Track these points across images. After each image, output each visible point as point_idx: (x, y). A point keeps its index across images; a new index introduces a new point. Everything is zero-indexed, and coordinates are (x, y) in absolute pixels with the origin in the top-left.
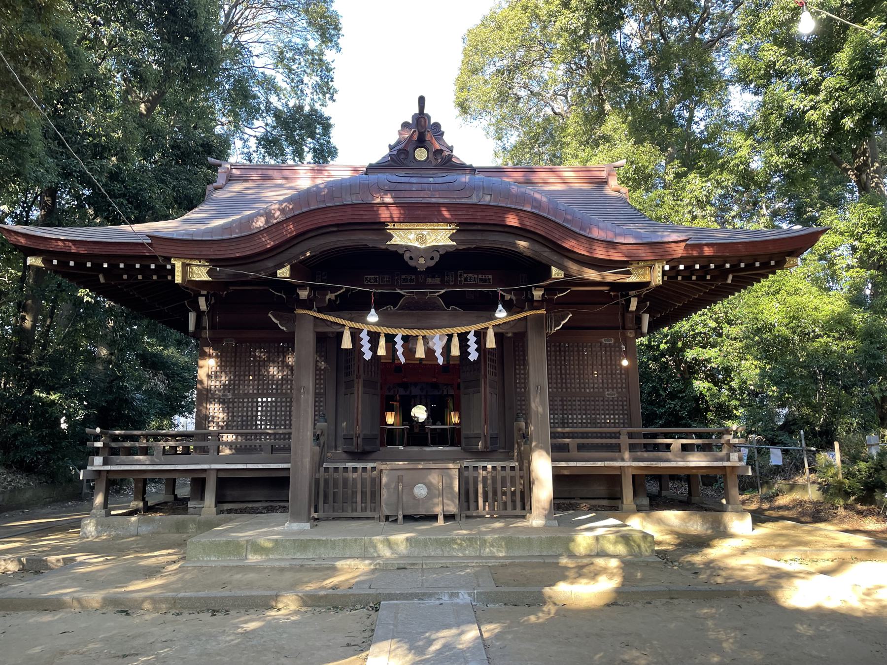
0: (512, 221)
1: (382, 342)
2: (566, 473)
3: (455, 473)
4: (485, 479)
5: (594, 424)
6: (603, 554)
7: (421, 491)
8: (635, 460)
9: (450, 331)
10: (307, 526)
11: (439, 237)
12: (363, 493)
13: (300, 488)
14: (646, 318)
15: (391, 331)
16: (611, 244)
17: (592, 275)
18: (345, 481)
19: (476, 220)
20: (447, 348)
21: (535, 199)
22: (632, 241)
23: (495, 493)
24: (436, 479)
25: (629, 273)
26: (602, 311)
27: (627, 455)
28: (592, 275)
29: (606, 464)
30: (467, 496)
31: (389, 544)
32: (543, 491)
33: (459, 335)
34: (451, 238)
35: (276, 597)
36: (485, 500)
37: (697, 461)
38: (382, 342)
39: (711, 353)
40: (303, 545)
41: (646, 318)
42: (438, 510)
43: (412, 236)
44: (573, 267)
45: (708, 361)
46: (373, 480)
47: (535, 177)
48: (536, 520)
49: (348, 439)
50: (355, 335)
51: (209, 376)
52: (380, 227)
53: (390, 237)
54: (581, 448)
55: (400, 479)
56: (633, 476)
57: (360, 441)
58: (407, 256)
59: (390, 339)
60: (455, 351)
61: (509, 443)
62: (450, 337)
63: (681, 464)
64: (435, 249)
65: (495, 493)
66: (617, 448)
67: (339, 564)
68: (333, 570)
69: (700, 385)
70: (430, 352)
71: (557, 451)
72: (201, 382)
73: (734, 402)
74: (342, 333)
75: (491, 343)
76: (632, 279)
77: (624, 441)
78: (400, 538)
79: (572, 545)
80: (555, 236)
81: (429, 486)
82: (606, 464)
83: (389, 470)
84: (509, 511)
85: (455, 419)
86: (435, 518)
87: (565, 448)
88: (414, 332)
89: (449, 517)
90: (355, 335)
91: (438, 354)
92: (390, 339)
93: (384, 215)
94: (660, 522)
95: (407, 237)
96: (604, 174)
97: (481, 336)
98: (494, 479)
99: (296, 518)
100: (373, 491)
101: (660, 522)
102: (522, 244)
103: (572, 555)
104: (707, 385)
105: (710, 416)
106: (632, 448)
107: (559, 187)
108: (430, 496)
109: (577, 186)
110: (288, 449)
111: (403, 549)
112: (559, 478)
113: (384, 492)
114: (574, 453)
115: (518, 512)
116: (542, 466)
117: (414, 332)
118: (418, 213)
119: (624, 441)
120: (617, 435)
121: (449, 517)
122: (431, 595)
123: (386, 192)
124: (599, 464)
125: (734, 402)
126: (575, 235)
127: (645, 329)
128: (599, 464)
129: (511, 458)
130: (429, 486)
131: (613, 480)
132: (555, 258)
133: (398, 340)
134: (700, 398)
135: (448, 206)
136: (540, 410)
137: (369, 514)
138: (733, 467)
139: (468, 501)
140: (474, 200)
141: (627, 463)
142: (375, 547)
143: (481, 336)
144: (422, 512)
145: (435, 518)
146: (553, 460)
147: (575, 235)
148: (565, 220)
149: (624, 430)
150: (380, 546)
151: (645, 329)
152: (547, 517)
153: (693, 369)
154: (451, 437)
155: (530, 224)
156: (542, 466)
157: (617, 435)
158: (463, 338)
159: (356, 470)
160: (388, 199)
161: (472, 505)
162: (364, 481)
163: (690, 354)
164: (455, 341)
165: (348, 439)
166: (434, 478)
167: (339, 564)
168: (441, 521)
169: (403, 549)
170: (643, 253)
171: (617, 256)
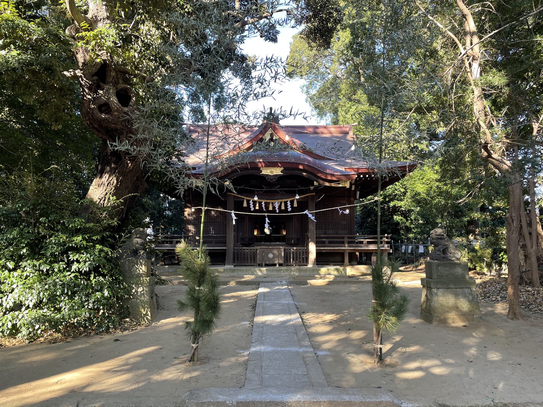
0: (301, 167)
1: (257, 205)
2: (324, 251)
3: (283, 250)
4: (293, 252)
5: (337, 234)
6: (329, 274)
7: (271, 256)
8: (350, 247)
9: (281, 201)
10: (233, 266)
11: (277, 171)
12: (251, 258)
13: (230, 256)
14: (358, 193)
15: (260, 201)
16: (332, 175)
17: (327, 184)
18: (244, 253)
19: (290, 168)
20: (280, 206)
21: (308, 160)
22: (339, 174)
23: (297, 258)
24: (276, 252)
25: (339, 184)
26: (335, 195)
27: (346, 245)
28: (327, 184)
29: (339, 248)
30: (287, 259)
31: (261, 271)
32: (312, 256)
33: (284, 202)
34: (281, 172)
35: (229, 282)
36: (293, 260)
37: (372, 247)
38: (257, 205)
39: (401, 204)
40: (233, 271)
41: (358, 193)
42: (276, 262)
43: (269, 171)
44: (321, 182)
45: (401, 207)
46: (254, 253)
47: (319, 131)
48: (310, 265)
49: (243, 239)
50: (248, 202)
51: (189, 215)
52: (259, 170)
53: (261, 172)
54: (330, 242)
55: (263, 252)
56: (349, 253)
57: (247, 240)
58: (267, 178)
59: (260, 204)
60: (283, 208)
61: (303, 242)
62: (281, 203)
63: (366, 248)
64: (276, 175)
65: (297, 258)
66: (343, 243)
67: (245, 276)
68: (243, 277)
69: (397, 218)
70: (274, 208)
71: (318, 244)
72: (186, 217)
73: (412, 226)
74: (243, 201)
75: (295, 205)
76: (340, 186)
77: (346, 240)
78: (264, 269)
79: (320, 272)
80: (315, 172)
81: (274, 254)
82: (339, 248)
83: (259, 249)
84: (302, 264)
85: (285, 233)
86: (275, 265)
87: (324, 242)
88: (268, 201)
89: (280, 265)
90: (248, 202)
91: (277, 209)
92: (260, 204)
93: (260, 165)
94: (357, 269)
95: (266, 171)
96: (347, 129)
97: (292, 202)
98: (296, 253)
99: (229, 264)
100: (255, 255)
101: (357, 269)
102: (304, 174)
103: (319, 274)
104: (400, 217)
105: (402, 232)
106: (349, 243)
107: (328, 135)
108: (274, 257)
109: (335, 135)
110: (226, 243)
111: (265, 272)
112: (318, 253)
113: (258, 256)
114: (327, 244)
115: (305, 264)
116: (312, 248)
117: (268, 201)
118: (271, 164)
119: (346, 240)
120: (343, 238)
121: (280, 265)
122: (274, 282)
123: (260, 158)
124: (336, 248)
125: (412, 226)
126: (322, 172)
127: (358, 197)
128: (336, 248)
129: (304, 247)
130: (274, 254)
131: (341, 254)
132: (315, 178)
133: (263, 203)
134: (398, 224)
135: (280, 163)
136: (312, 228)
137: (252, 264)
138: (386, 250)
139: (287, 260)
140: (289, 161)
141: (346, 247)
142: (256, 272)
143: (292, 202)
144: (271, 263)
145: (275, 265)
146: (316, 247)
147: (322, 172)
148: (318, 167)
149: (346, 236)
150: (258, 271)
151: (358, 197)
152: (313, 264)
153: (396, 210)
154: (282, 239)
155: (306, 168)
156: (312, 248)
157: (343, 238)
158: (286, 203)
159: (247, 250)
160: (261, 160)
161: (289, 261)
162: (251, 253)
163: (392, 204)
164: (283, 204)
165: (243, 239)
166: (275, 252)
167: (245, 276)
168: (277, 266)
169: (265, 272)
170: (343, 178)
171: (334, 179)
